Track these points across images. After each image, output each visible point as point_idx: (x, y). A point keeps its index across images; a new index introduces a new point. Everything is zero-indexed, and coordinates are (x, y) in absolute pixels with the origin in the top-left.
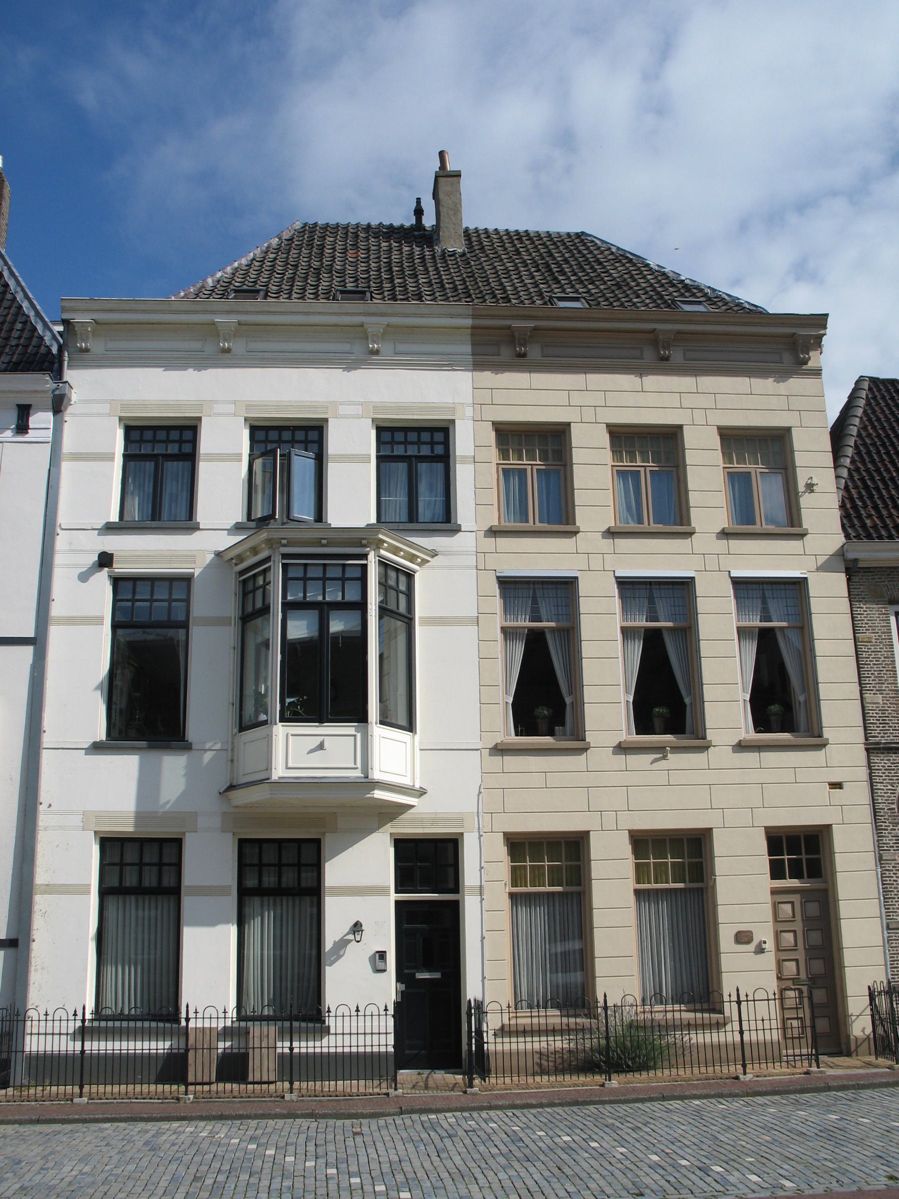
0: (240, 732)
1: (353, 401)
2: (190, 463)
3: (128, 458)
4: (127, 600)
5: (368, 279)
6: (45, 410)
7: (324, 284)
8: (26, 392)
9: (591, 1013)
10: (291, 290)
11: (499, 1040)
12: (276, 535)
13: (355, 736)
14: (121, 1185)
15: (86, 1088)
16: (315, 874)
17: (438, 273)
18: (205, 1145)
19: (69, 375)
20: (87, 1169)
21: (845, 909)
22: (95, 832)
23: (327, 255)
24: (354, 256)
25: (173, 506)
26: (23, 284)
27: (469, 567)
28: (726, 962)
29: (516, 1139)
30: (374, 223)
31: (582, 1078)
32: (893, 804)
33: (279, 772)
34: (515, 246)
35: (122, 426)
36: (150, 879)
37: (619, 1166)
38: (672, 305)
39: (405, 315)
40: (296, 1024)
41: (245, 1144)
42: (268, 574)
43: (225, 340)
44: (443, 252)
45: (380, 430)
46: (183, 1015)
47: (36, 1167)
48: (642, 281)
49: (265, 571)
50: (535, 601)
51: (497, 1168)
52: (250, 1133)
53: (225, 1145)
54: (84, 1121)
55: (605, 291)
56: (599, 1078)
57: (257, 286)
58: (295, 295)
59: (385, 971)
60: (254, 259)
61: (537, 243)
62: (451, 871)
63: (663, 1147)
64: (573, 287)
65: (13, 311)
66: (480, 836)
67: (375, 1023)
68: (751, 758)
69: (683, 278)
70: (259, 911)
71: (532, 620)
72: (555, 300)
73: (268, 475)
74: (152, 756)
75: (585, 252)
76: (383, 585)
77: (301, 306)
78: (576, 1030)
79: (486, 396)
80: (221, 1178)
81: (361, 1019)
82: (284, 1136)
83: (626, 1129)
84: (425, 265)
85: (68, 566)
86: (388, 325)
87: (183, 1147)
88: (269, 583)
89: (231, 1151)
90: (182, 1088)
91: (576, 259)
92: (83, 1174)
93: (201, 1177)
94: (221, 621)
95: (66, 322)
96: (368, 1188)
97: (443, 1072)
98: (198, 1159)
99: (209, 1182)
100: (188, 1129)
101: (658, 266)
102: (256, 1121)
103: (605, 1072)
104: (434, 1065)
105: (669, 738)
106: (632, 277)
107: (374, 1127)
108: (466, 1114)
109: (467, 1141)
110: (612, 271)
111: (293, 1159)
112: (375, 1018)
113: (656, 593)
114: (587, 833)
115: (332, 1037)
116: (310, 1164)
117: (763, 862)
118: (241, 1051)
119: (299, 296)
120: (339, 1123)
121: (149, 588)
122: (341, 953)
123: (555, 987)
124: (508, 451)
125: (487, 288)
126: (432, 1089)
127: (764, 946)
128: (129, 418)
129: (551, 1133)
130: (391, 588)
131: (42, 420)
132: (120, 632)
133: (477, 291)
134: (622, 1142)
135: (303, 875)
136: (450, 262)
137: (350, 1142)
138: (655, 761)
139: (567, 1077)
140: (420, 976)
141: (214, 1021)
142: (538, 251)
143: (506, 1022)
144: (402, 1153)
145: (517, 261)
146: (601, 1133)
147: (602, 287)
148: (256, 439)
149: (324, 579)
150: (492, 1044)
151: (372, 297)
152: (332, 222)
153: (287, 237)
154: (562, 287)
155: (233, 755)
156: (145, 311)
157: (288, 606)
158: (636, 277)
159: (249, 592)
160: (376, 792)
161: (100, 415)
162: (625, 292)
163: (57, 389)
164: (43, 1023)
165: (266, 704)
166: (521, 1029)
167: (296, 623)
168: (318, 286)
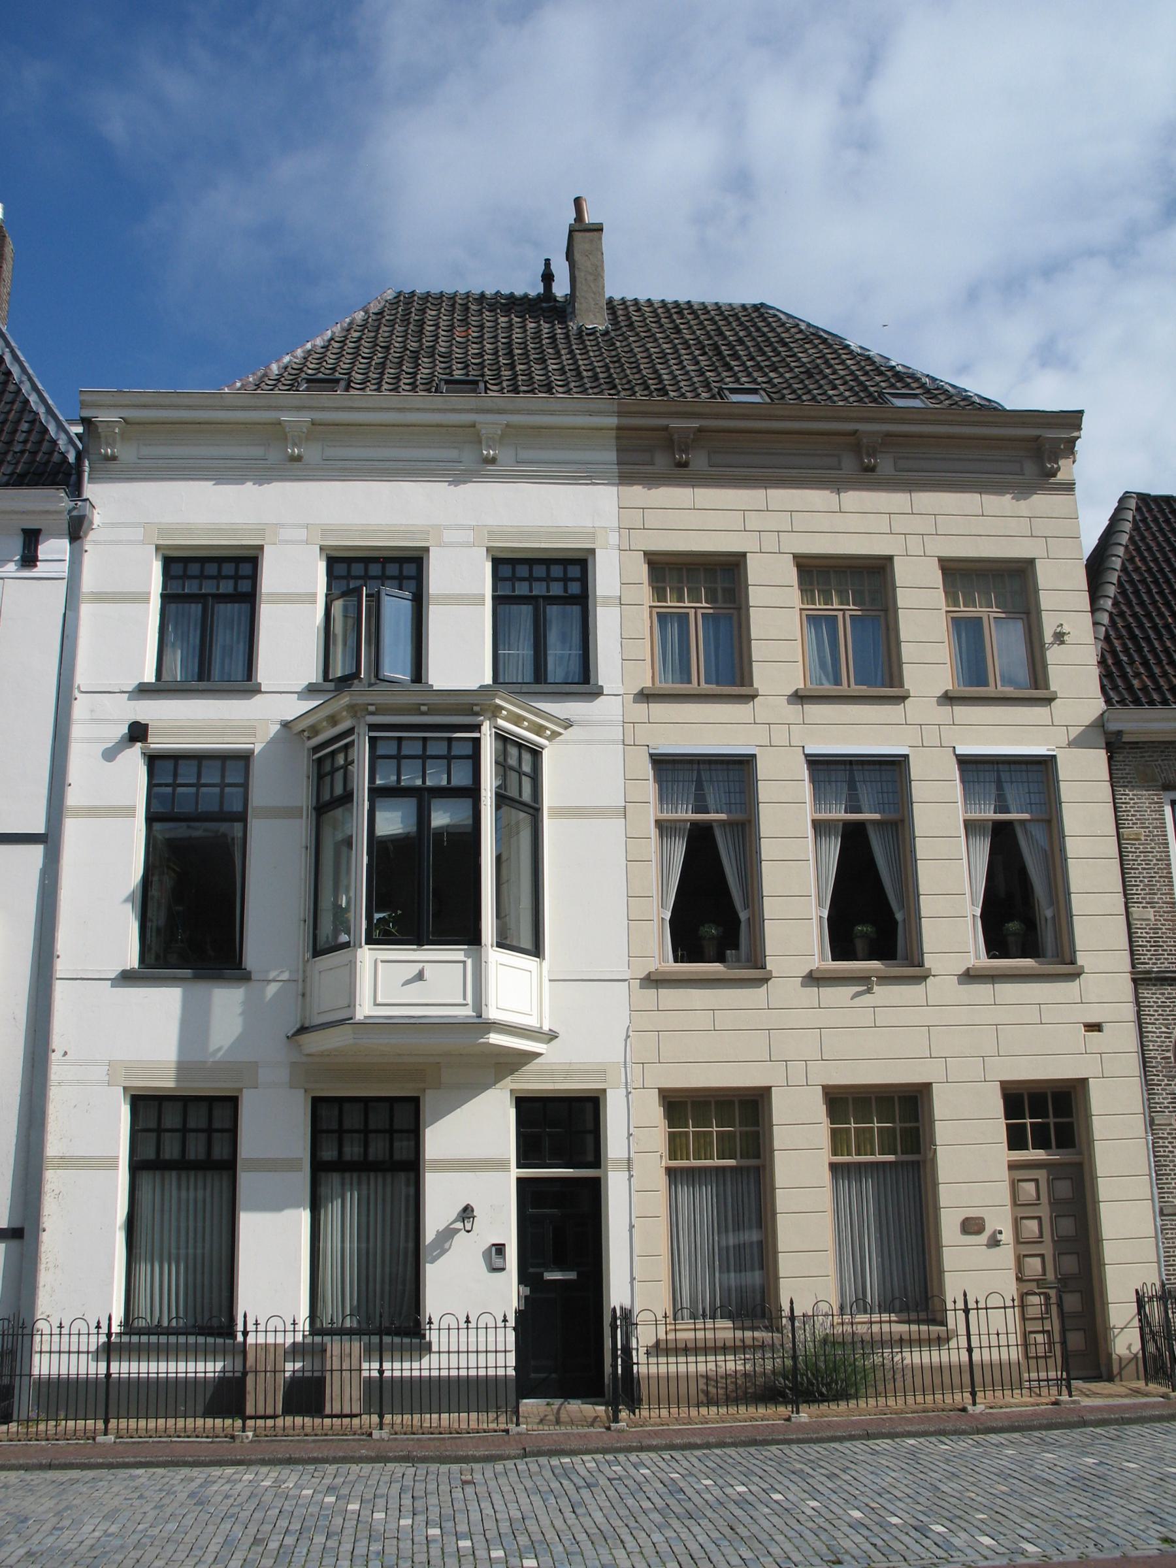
0: (314, 957)
1: (462, 524)
2: (248, 606)
3: (167, 598)
4: (167, 785)
5: (481, 365)
6: (59, 536)
7: (424, 372)
8: (34, 512)
9: (773, 1325)
10: (381, 379)
11: (653, 1360)
12: (361, 700)
13: (464, 962)
14: (159, 1550)
15: (113, 1423)
16: (412, 1143)
17: (573, 357)
18: (268, 1498)
19: (90, 490)
20: (114, 1529)
21: (1106, 1189)
22: (125, 1088)
23: (428, 334)
24: (463, 334)
25: (227, 661)
26: (30, 371)
27: (614, 742)
28: (950, 1259)
29: (675, 1490)
30: (490, 291)
31: (762, 1410)
32: (1168, 1051)
33: (364, 1009)
34: (673, 321)
35: (160, 557)
36: (196, 1149)
37: (810, 1524)
38: (879, 398)
39: (530, 412)
40: (387, 1339)
41: (320, 1496)
42: (350, 751)
43: (295, 445)
44: (580, 330)
45: (497, 562)
46: (240, 1327)
47: (48, 1527)
48: (840, 367)
49: (347, 747)
50: (699, 786)
51: (650, 1528)
52: (327, 1481)
53: (294, 1497)
54: (110, 1466)
55: (791, 381)
56: (783, 1410)
57: (337, 374)
58: (385, 386)
59: (503, 1269)
60: (332, 339)
61: (702, 317)
62: (590, 1139)
63: (867, 1500)
64: (749, 375)
65: (17, 406)
66: (628, 1093)
67: (491, 1338)
68: (983, 991)
69: (893, 364)
70: (339, 1191)
71: (696, 810)
72: (727, 392)
73: (350, 622)
74: (199, 988)
75: (765, 329)
76: (502, 765)
77: (394, 400)
78: (754, 1347)
79: (635, 518)
80: (289, 1540)
81: (472, 1332)
82: (372, 1486)
83: (818, 1477)
84: (555, 347)
85: (89, 740)
86: (507, 426)
87: (239, 1500)
88: (353, 762)
89: (302, 1506)
90: (239, 1423)
91: (754, 339)
92: (109, 1535)
93: (263, 1539)
94: (289, 813)
95: (86, 422)
96: (481, 1553)
97: (579, 1402)
98: (258, 1515)
99: (273, 1545)
100: (246, 1477)
101: (861, 347)
102: (335, 1466)
103: (791, 1402)
104: (568, 1393)
105: (875, 965)
106: (826, 362)
107: (489, 1474)
108: (609, 1457)
109: (611, 1493)
110: (800, 355)
111: (383, 1515)
112: (491, 1332)
113: (858, 776)
114: (768, 1089)
115: (434, 1357)
116: (406, 1522)
117: (999, 1128)
118: (316, 1374)
119: (391, 387)
120: (444, 1468)
121: (195, 769)
122: (447, 1246)
123: (727, 1291)
124: (664, 589)
125: (637, 376)
126: (566, 1424)
127: (999, 1237)
128: (169, 547)
129: (720, 1482)
130: (512, 768)
131: (55, 549)
132: (157, 826)
133: (624, 381)
134: (814, 1493)
135: (396, 1144)
136: (588, 343)
137: (458, 1494)
138: (857, 995)
139: (742, 1409)
140: (549, 1276)
141: (280, 1335)
142: (704, 328)
143: (662, 1336)
144: (526, 1507)
145: (677, 341)
146: (787, 1482)
147: (788, 375)
148: (335, 574)
149: (424, 757)
150: (644, 1365)
151: (486, 389)
152: (435, 290)
153: (376, 310)
154: (735, 375)
155: (304, 988)
156: (189, 407)
157: (377, 793)
158: (832, 362)
159: (326, 775)
160: (492, 1035)
161: (130, 542)
162: (817, 382)
163: (74, 508)
164: (56, 1338)
165: (348, 921)
166: (681, 1345)
167: (388, 815)
168: (416, 374)
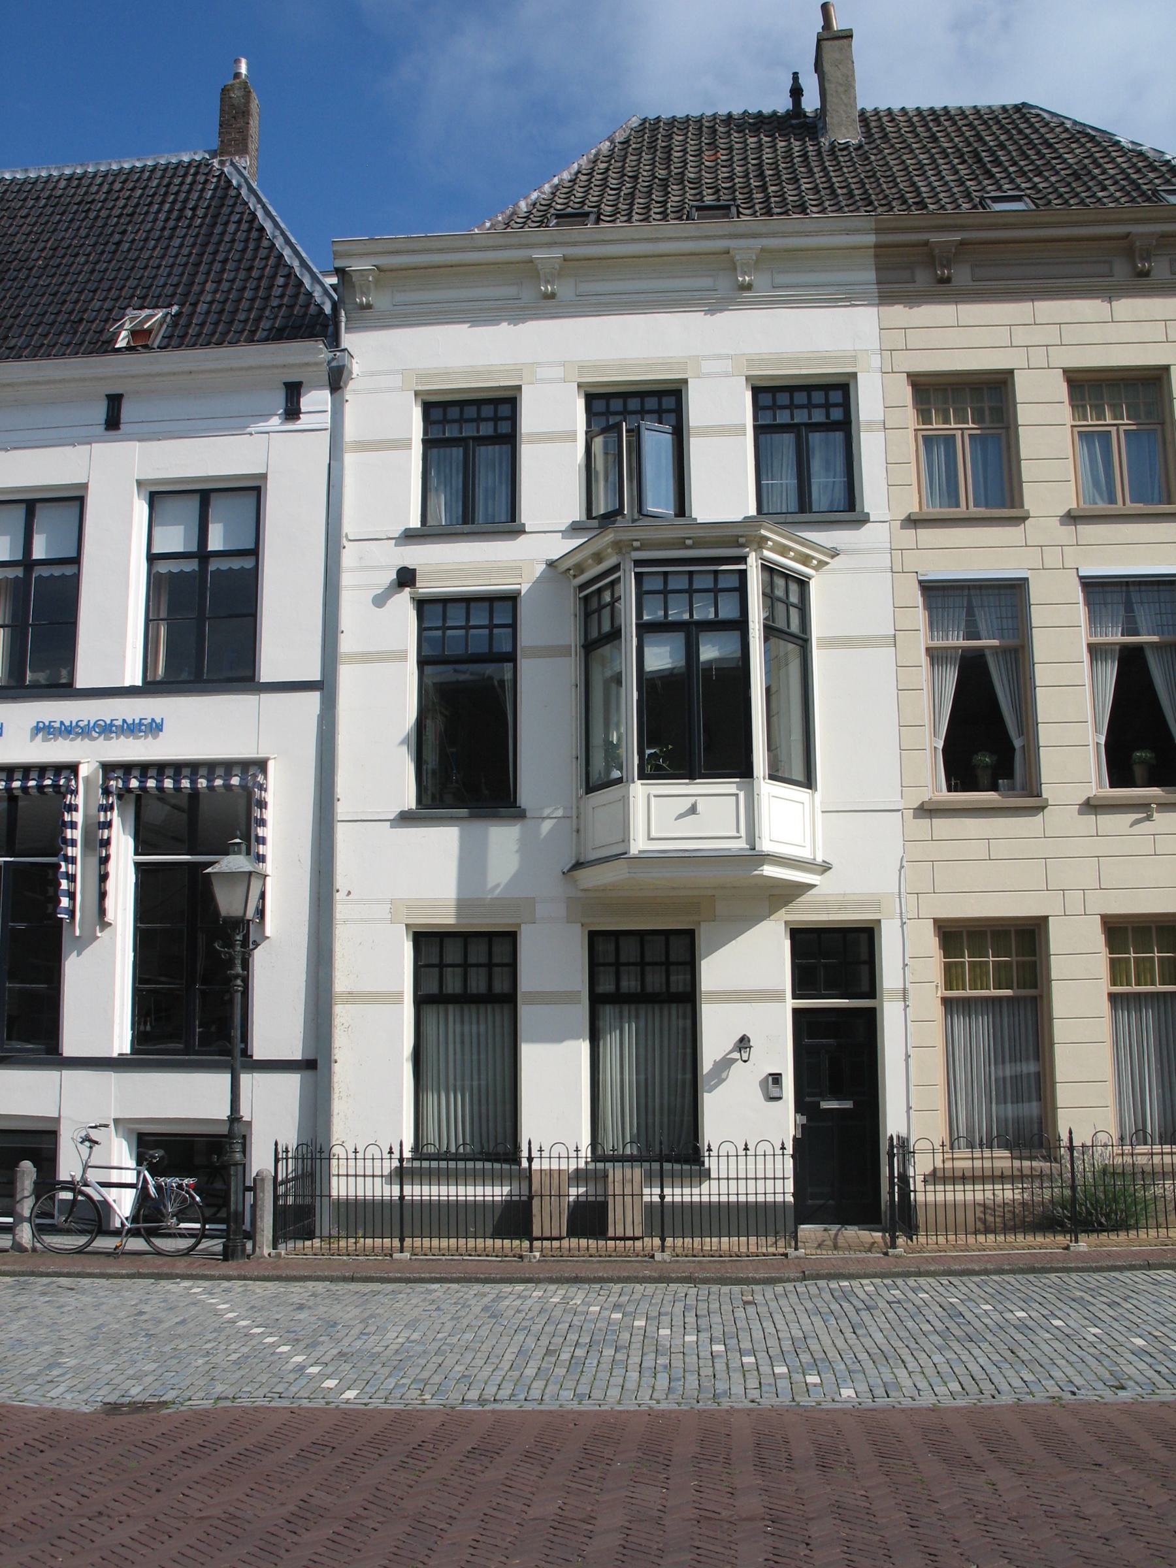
0: (587, 793)
1: (718, 353)
3: (429, 443)
4: (437, 629)
5: (732, 189)
6: (319, 387)
7: (673, 200)
10: (631, 210)
11: (930, 1188)
12: (625, 536)
13: (737, 795)
14: (458, 1357)
15: (408, 1242)
16: (688, 977)
17: (827, 175)
18: (557, 1313)
19: (348, 340)
20: (415, 1336)
22: (407, 925)
23: (676, 160)
24: (713, 158)
25: (490, 502)
26: (283, 226)
29: (954, 1314)
30: (737, 111)
31: (1040, 1239)
33: (639, 844)
34: (929, 129)
35: (420, 403)
36: (477, 984)
37: (1092, 1350)
38: (1153, 197)
39: (785, 235)
40: (667, 1166)
41: (607, 1313)
42: (616, 587)
43: (547, 282)
44: (832, 145)
45: (757, 391)
46: (525, 1153)
47: (355, 1332)
48: (1110, 166)
49: (613, 584)
50: (970, 612)
51: (931, 1350)
52: (613, 1299)
53: (582, 1313)
54: (408, 1281)
55: (1057, 185)
56: (1061, 1239)
57: (586, 207)
58: (636, 217)
59: (780, 1098)
60: (579, 172)
61: (960, 123)
62: (865, 969)
63: (1149, 1329)
64: (1012, 181)
65: (272, 261)
66: (903, 924)
67: (770, 1166)
69: (1168, 157)
70: (618, 1024)
71: (968, 637)
72: (989, 201)
73: (611, 458)
74: (477, 826)
75: (1028, 131)
76: (769, 596)
77: (646, 230)
78: (1032, 1176)
79: (897, 339)
80: (580, 1352)
81: (751, 1159)
82: (657, 1304)
83: (1099, 1305)
84: (808, 165)
86: (762, 250)
87: (530, 1315)
88: (620, 598)
89: (590, 1321)
90: (526, 1244)
91: (1016, 143)
92: (412, 1342)
93: (555, 1351)
94: (558, 651)
95: (340, 272)
96: (765, 1369)
97: (856, 1228)
98: (549, 1329)
99: (565, 1356)
100: (535, 1294)
101: (1132, 142)
102: (620, 1285)
103: (1070, 1232)
104: (845, 1220)
105: (1155, 791)
106: (1095, 162)
107: (769, 1295)
108: (888, 1281)
109: (891, 1315)
110: (1066, 156)
111: (668, 1332)
112: (769, 1159)
113: (1135, 597)
114: (1045, 919)
115: (714, 1183)
116: (691, 1338)
118: (599, 1199)
119: (641, 217)
120: (725, 1289)
121: (464, 611)
122: (724, 1075)
123: (1003, 1122)
124: (929, 411)
125: (894, 191)
126: (843, 1249)
128: (429, 392)
129: (1000, 1307)
130: (779, 600)
131: (315, 400)
132: (428, 669)
133: (881, 196)
134: (1095, 1320)
135: (673, 978)
136: (842, 159)
137: (740, 1313)
138: (1136, 822)
139: (1020, 1237)
141: (564, 1162)
142: (962, 134)
143: (939, 1165)
144: (807, 1328)
145: (934, 151)
146: (1067, 1309)
147: (1053, 179)
148: (594, 410)
149: (690, 591)
150: (923, 1194)
151: (739, 213)
152: (680, 114)
153: (622, 139)
154: (996, 182)
155: (578, 824)
156: (440, 251)
157: (644, 628)
158: (1101, 161)
159: (593, 612)
160: (765, 867)
162: (1085, 183)
163: (333, 359)
164: (352, 1163)
165: (619, 757)
166: (959, 1174)
167: (656, 650)
168: (666, 202)
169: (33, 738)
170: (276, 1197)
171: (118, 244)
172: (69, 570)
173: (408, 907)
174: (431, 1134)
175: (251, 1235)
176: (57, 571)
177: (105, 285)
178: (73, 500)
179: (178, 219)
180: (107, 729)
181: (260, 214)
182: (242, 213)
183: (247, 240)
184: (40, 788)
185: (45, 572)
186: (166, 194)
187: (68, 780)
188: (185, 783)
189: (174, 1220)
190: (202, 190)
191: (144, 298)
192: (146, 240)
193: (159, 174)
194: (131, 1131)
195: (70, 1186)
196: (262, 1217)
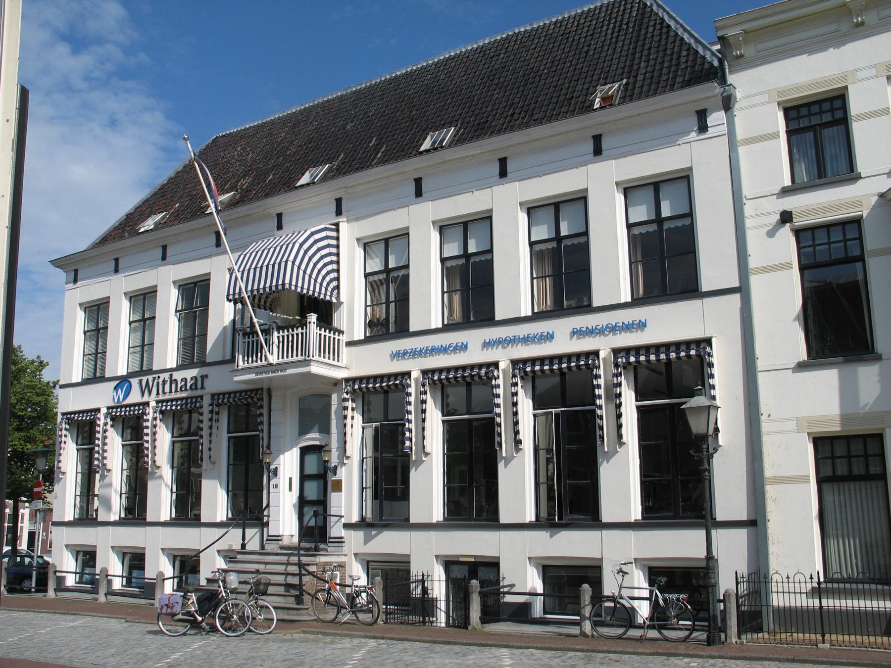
2: (843, 126)
4: (809, 246)
15: (827, 636)
19: (731, 79)
26: (681, 21)
43: (858, 15)
65: (677, 43)
74: (849, 368)
85: (757, 227)
95: (722, 40)
118: (753, 609)
131: (716, 118)
161: (761, 104)
164: (786, 585)
169: (571, 339)
170: (738, 607)
171: (587, 52)
172: (582, 240)
173: (808, 422)
174: (834, 567)
175: (724, 629)
176: (575, 241)
177: (583, 76)
178: (581, 199)
179: (619, 31)
180: (613, 329)
181: (666, 18)
182: (656, 20)
183: (661, 34)
184: (578, 366)
185: (568, 242)
186: (610, 19)
187: (594, 360)
188: (663, 356)
189: (675, 620)
190: (630, 12)
191: (606, 78)
192: (603, 46)
193: (604, 9)
194: (644, 565)
195: (612, 599)
196: (730, 619)
